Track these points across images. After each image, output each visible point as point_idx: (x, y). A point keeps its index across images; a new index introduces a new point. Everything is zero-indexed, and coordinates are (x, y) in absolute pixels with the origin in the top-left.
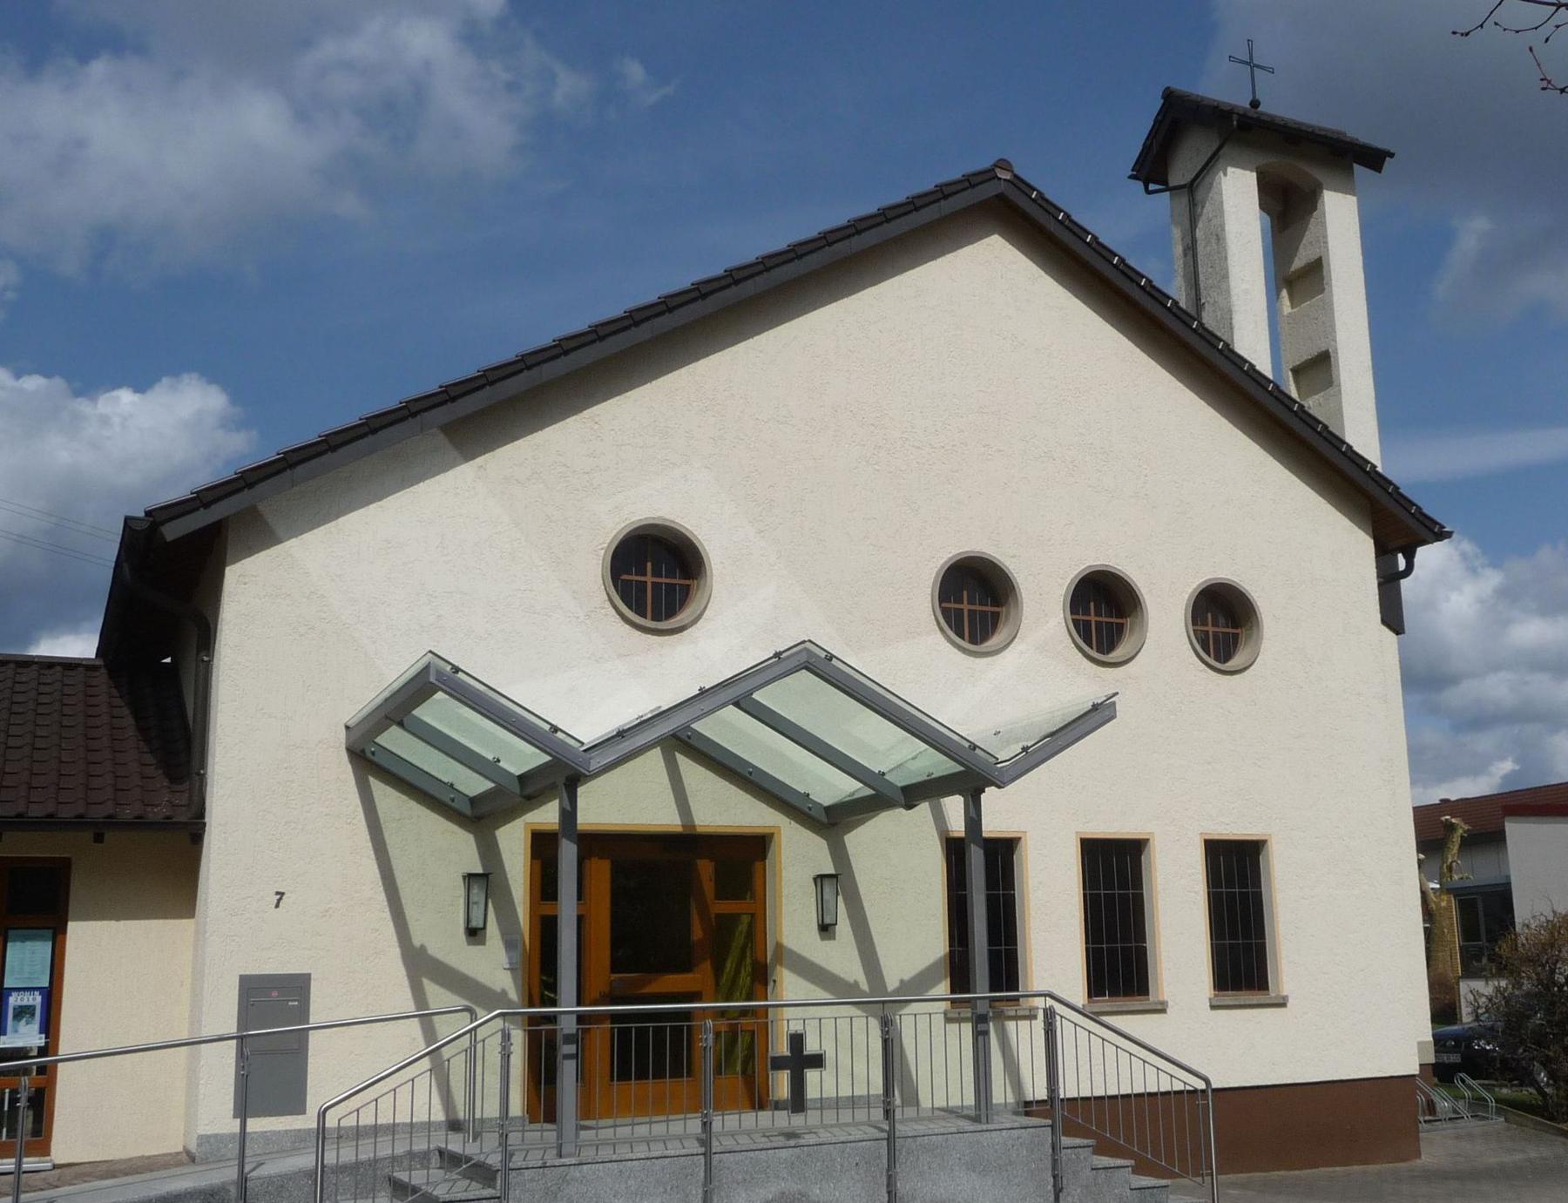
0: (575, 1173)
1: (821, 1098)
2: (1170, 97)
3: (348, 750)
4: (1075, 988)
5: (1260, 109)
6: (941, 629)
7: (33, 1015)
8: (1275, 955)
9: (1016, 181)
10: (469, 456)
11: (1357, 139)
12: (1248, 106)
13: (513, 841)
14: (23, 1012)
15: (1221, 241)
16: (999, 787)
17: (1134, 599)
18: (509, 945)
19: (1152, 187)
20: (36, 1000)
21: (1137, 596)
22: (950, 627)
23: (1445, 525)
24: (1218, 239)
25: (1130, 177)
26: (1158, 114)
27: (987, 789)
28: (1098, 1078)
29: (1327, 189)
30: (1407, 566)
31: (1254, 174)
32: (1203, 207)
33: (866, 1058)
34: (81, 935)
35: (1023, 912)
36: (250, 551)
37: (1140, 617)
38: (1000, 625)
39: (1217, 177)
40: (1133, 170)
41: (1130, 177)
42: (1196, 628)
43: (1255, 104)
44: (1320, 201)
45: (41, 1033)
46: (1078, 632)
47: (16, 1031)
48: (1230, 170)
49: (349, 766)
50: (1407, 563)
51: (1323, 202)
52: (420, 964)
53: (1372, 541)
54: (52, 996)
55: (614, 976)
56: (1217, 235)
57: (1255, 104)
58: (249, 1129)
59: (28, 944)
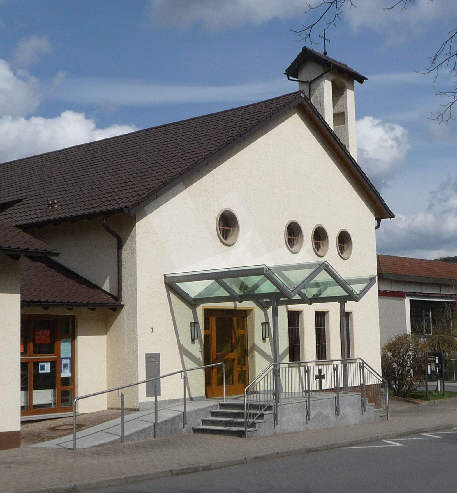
0: (285, 407)
1: (262, 391)
2: (305, 49)
3: (165, 283)
4: (314, 357)
5: (327, 55)
6: (287, 245)
7: (68, 366)
8: (330, 349)
9: (305, 97)
10: (186, 188)
11: (347, 66)
12: (323, 54)
13: (200, 311)
14: (66, 365)
15: (322, 106)
16: (356, 301)
17: (325, 235)
18: (201, 344)
19: (291, 78)
20: (68, 362)
21: (327, 234)
22: (289, 245)
23: (394, 213)
24: (321, 105)
25: (285, 73)
26: (300, 54)
27: (348, 302)
28: (373, 382)
29: (348, 89)
30: (378, 225)
31: (331, 83)
32: (314, 92)
33: (125, 385)
34: (82, 341)
35: (303, 334)
36: (142, 218)
37: (326, 240)
38: (295, 243)
39: (321, 83)
40: (286, 71)
41: (285, 73)
42: (340, 245)
43: (325, 53)
44: (345, 92)
45: (70, 372)
46: (315, 246)
47: (64, 372)
48: (326, 81)
49: (165, 288)
50: (378, 223)
51: (346, 93)
52: (183, 351)
53: (49, 119)
54: (73, 359)
55: (218, 353)
56: (320, 103)
57: (325, 53)
58: (158, 400)
59: (65, 343)
